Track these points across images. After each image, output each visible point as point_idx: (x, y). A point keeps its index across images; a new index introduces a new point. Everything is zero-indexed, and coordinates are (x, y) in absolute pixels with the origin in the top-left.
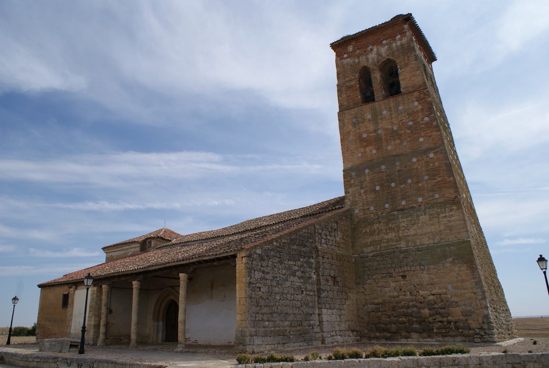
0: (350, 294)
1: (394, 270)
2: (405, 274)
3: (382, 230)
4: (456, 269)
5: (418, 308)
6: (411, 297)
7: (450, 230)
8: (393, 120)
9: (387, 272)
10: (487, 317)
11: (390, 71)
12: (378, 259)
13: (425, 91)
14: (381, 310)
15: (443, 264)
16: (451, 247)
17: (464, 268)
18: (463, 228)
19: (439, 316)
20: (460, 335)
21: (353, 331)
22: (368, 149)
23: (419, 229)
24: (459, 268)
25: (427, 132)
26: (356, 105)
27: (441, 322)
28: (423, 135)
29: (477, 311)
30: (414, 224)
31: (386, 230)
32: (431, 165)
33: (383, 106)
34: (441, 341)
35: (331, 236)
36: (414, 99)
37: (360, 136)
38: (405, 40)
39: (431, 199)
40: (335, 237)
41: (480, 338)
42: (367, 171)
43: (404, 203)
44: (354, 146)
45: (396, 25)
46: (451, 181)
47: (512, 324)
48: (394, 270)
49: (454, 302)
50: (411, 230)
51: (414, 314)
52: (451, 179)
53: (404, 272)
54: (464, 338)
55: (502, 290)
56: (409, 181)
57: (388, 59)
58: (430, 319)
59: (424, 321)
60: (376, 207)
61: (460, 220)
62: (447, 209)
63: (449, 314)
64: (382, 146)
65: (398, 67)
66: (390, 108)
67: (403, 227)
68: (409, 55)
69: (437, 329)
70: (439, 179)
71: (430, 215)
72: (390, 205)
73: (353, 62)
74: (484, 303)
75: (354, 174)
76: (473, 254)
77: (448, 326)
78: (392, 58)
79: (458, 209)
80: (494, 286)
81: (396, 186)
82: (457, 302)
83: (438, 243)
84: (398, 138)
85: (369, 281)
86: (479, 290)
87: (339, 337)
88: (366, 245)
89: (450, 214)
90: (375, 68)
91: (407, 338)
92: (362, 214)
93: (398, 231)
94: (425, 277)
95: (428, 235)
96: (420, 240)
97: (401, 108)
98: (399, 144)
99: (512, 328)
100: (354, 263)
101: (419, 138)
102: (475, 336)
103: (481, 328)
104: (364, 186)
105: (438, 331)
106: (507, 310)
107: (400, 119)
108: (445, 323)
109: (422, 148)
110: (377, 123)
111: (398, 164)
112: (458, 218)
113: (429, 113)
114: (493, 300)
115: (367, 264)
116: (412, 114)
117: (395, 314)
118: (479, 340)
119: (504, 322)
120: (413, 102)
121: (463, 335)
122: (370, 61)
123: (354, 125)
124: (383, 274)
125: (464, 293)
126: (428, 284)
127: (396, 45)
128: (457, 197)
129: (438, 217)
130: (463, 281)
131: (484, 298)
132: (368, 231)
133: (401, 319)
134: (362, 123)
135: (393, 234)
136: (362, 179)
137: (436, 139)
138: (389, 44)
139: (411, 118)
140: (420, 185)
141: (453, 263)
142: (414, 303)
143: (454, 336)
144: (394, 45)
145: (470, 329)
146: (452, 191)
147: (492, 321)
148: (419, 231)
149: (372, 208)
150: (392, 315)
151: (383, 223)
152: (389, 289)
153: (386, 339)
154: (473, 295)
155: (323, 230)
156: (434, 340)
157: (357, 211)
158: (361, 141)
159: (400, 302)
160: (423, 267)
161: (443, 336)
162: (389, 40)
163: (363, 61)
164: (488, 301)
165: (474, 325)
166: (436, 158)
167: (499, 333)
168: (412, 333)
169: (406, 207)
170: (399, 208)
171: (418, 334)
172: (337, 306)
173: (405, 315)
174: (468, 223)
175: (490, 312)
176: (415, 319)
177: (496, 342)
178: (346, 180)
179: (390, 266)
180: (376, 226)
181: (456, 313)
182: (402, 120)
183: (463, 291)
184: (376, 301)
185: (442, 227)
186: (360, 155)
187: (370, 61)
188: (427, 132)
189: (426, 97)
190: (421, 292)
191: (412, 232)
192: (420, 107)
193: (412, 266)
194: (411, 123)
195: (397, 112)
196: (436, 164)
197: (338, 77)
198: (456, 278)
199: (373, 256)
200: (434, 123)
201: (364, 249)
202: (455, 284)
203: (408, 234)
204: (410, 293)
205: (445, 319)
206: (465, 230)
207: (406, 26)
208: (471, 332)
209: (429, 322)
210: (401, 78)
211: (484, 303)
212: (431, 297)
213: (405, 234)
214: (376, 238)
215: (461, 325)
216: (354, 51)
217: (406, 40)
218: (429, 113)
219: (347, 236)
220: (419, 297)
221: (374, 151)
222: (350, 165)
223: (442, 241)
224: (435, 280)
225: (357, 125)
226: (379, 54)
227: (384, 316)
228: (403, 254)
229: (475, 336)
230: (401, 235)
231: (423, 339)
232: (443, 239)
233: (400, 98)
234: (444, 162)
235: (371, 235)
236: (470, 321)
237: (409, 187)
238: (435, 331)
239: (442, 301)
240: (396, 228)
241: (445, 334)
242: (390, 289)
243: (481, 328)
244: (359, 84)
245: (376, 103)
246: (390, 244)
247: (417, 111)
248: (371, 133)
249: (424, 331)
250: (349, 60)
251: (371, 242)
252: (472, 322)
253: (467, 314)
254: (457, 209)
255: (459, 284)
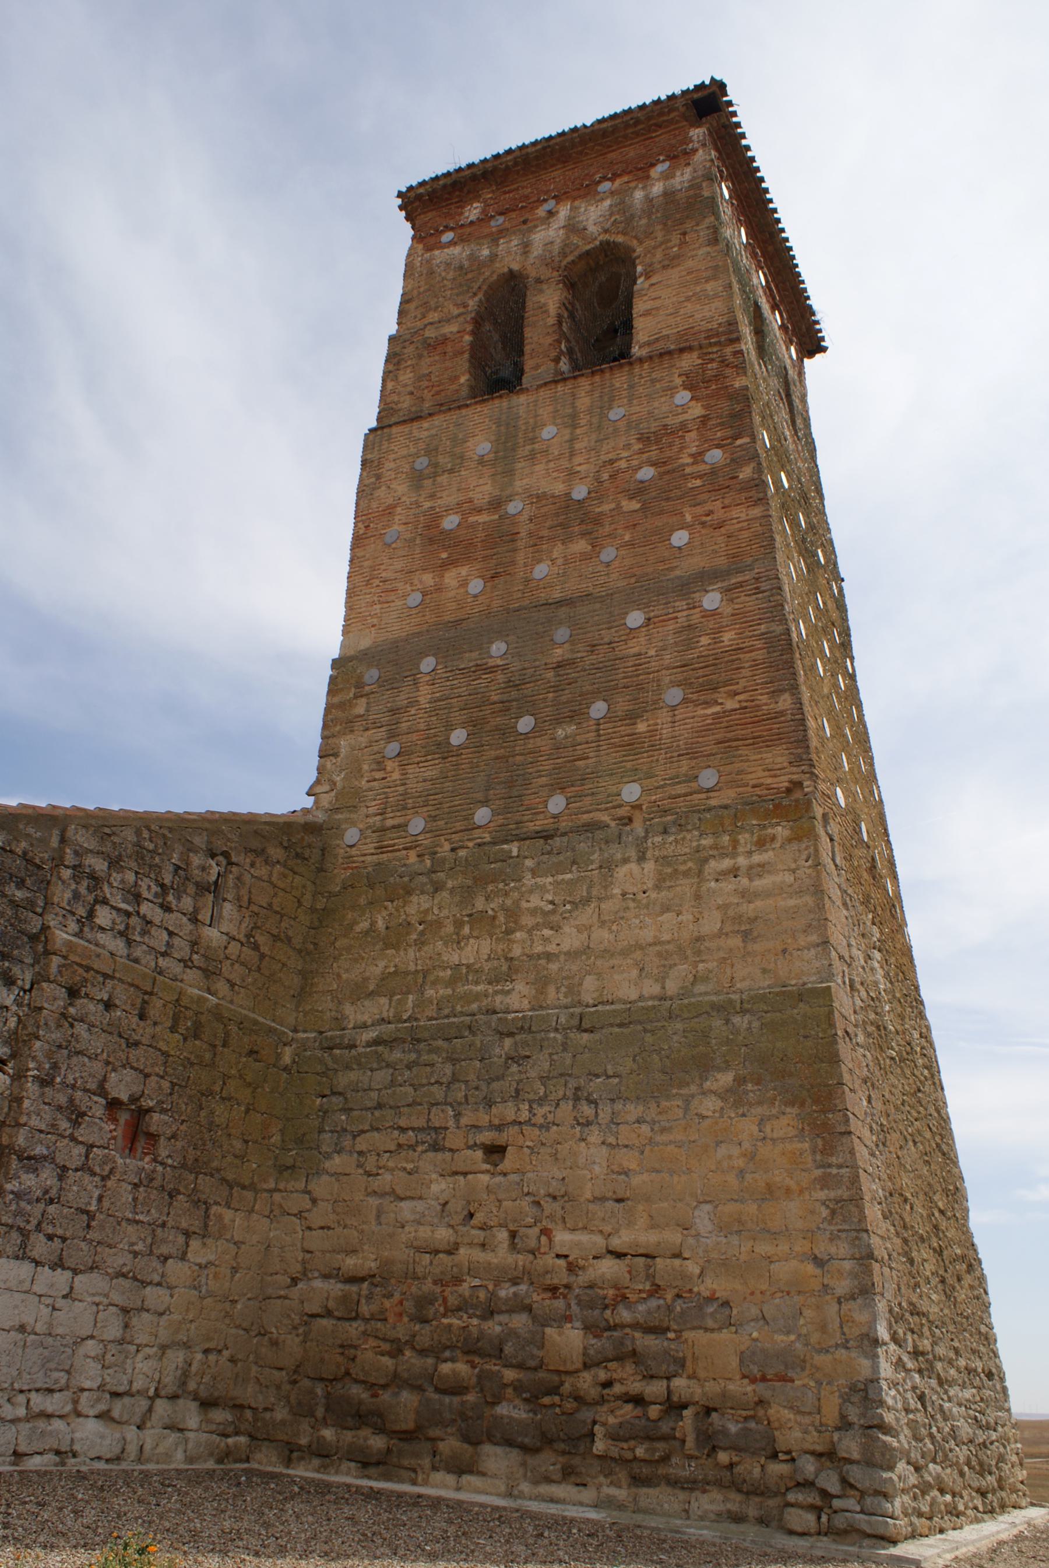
0: (228, 1215)
1: (458, 1116)
2: (501, 1139)
3: (439, 924)
4: (748, 1127)
5: (534, 1319)
6: (511, 1259)
7: (746, 935)
8: (578, 460)
9: (421, 1123)
10: (865, 1393)
11: (602, 288)
12: (397, 1055)
13: (729, 350)
14: (365, 1309)
15: (688, 1100)
16: (736, 1020)
17: (785, 1124)
18: (807, 929)
19: (630, 1368)
20: (719, 1484)
21: (206, 1404)
22: (451, 578)
23: (603, 923)
24: (761, 1123)
25: (708, 507)
26: (446, 406)
27: (638, 1400)
28: (688, 518)
29: (819, 1359)
30: (586, 901)
31: (459, 924)
32: (705, 640)
33: (544, 411)
34: (621, 1507)
35: (167, 908)
36: (678, 381)
37: (434, 519)
38: (682, 178)
39: (680, 789)
40: (194, 920)
41: (818, 1510)
42: (428, 664)
43: (557, 804)
44: (398, 565)
45: (659, 126)
46: (782, 713)
47: (1004, 1440)
48: (458, 1116)
49: (711, 1299)
50: (567, 929)
51: (508, 1349)
52: (785, 702)
53: (499, 1128)
54: (734, 1502)
55: (982, 1280)
56: (598, 709)
57: (607, 248)
58: (586, 1382)
59: (554, 1390)
60: (434, 818)
61: (800, 893)
62: (743, 838)
63: (682, 1363)
64: (513, 563)
65: (639, 269)
66: (574, 416)
67: (533, 912)
68: (688, 225)
69: (614, 1437)
70: (731, 704)
71: (663, 860)
72: (495, 813)
73: (472, 257)
74: (862, 1317)
75: (372, 675)
76: (835, 1060)
77: (665, 1427)
78: (620, 239)
79: (796, 837)
80: (939, 1252)
81: (536, 731)
82: (726, 1304)
83: (681, 996)
84: (583, 534)
85: (336, 1162)
86: (842, 1249)
87: (92, 1426)
88: (360, 992)
89: (757, 858)
90: (546, 273)
91: (461, 1468)
92: (370, 848)
93: (509, 932)
94: (591, 1161)
95: (638, 955)
96: (599, 975)
97: (616, 414)
98: (585, 557)
99: (1001, 1459)
100: (286, 1069)
101: (672, 531)
102: (791, 1497)
103: (829, 1456)
104: (404, 726)
105: (614, 1452)
106: (990, 1375)
107: (604, 458)
108: (654, 1411)
109: (678, 573)
110: (510, 473)
111: (562, 634)
112: (789, 878)
113: (729, 432)
114: (915, 1312)
115: (344, 1079)
116: (657, 438)
117: (425, 1335)
118: (810, 1518)
119: (965, 1430)
120: (671, 390)
121: (736, 1485)
122: (537, 251)
123: (417, 479)
124: (403, 1130)
125: (770, 1259)
126: (603, 1199)
127: (646, 197)
128: (799, 784)
129: (700, 873)
130: (770, 1192)
131: (865, 1291)
132: (381, 924)
133: (446, 1368)
134: (451, 471)
135: (485, 946)
136: (402, 700)
137: (745, 534)
138: (623, 193)
139: (654, 454)
140: (642, 727)
141: (734, 1096)
142: (523, 1288)
143: (690, 1485)
144: (639, 195)
145: (774, 1456)
146: (778, 756)
147: (889, 1418)
148: (602, 936)
149: (417, 825)
150: (411, 1343)
151: (452, 891)
152: (420, 1206)
153: (365, 1465)
154: (810, 1268)
155: (115, 863)
156: (588, 1495)
157: (351, 835)
158: (431, 541)
159: (458, 1281)
160: (587, 1110)
161: (637, 1481)
162: (626, 179)
163: (509, 254)
164: (881, 1306)
165: (795, 1432)
166: (729, 610)
167: (924, 1488)
168: (487, 1448)
169: (564, 825)
170: (532, 827)
171: (515, 1454)
172: (119, 1260)
173: (472, 1348)
174: (838, 918)
175: (886, 1370)
176: (510, 1375)
177: (894, 1542)
178: (336, 700)
179: (438, 1092)
180: (418, 904)
181: (716, 1361)
182: (612, 462)
183: (764, 1248)
184: (350, 1263)
185: (711, 923)
186: (415, 598)
187: (537, 251)
188: (708, 507)
189: (728, 371)
190: (562, 1238)
191: (570, 939)
192: (697, 410)
193: (542, 1101)
194: (647, 473)
195: (599, 427)
196: (728, 637)
197: (401, 313)
198: (741, 1173)
199: (377, 1042)
200: (746, 473)
201: (348, 1009)
202: (731, 1208)
203: (552, 948)
204: (513, 1235)
205: (655, 1389)
206: (814, 938)
207: (698, 133)
208: (778, 1468)
209: (578, 1399)
210: (639, 306)
211: (862, 1317)
212: (608, 1267)
213: (539, 949)
214: (409, 958)
215: (733, 1428)
216: (485, 219)
217: (687, 176)
218: (729, 432)
219: (276, 938)
220: (549, 1260)
221: (476, 586)
222: (365, 643)
223: (700, 988)
224: (636, 1180)
225: (427, 483)
226: (572, 228)
227: (372, 1342)
228: (508, 1042)
229: (791, 1497)
230: (517, 951)
231: (536, 1483)
232: (706, 979)
233: (620, 379)
234: (763, 628)
235: (387, 946)
236: (778, 1412)
237: (591, 736)
238: (600, 1446)
239: (656, 1290)
240: (502, 919)
241: (646, 1470)
242: (409, 1208)
243: (829, 1456)
244: (472, 333)
245: (522, 399)
246: (461, 989)
247: (683, 427)
248: (479, 511)
249: (547, 1441)
250: (456, 250)
251: (385, 977)
252: (787, 1414)
253: (770, 1371)
254: (790, 840)
255: (752, 1208)
